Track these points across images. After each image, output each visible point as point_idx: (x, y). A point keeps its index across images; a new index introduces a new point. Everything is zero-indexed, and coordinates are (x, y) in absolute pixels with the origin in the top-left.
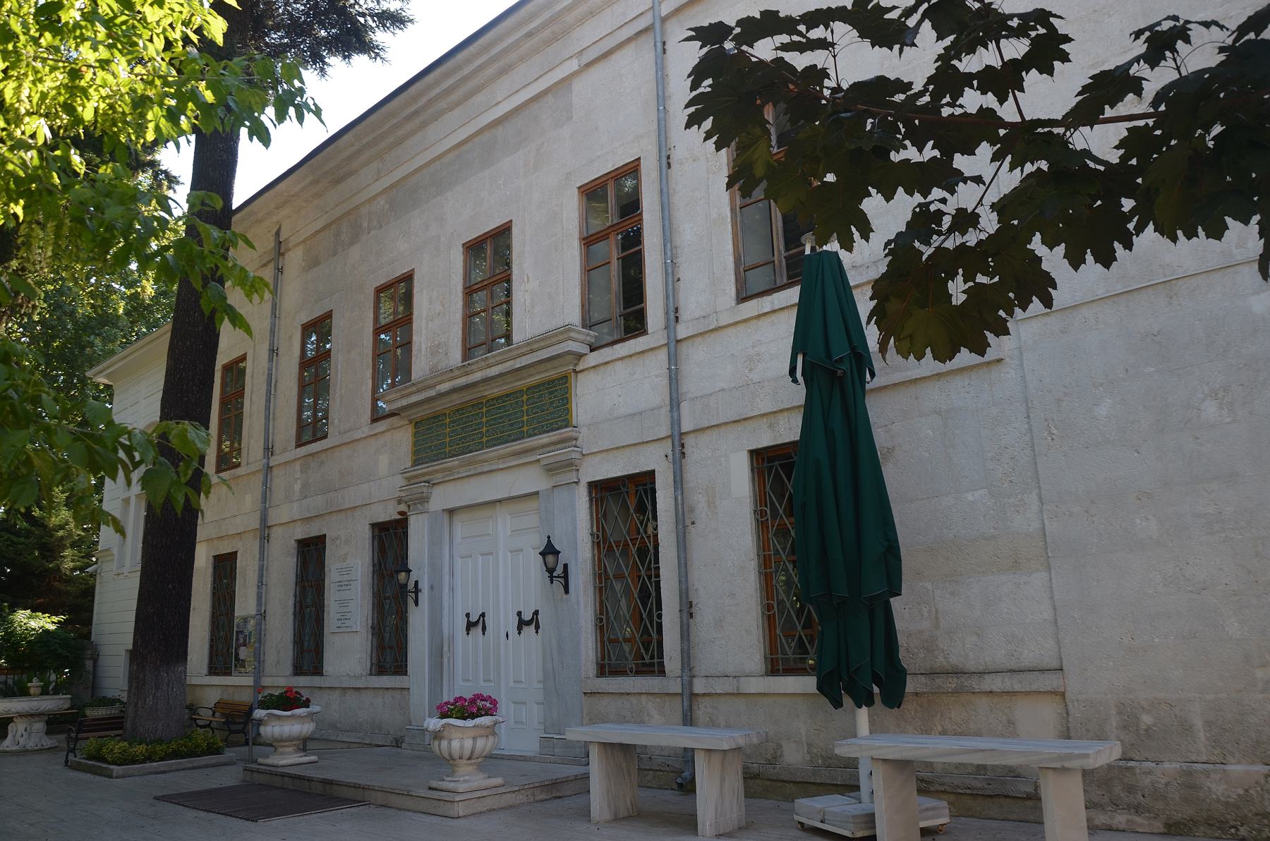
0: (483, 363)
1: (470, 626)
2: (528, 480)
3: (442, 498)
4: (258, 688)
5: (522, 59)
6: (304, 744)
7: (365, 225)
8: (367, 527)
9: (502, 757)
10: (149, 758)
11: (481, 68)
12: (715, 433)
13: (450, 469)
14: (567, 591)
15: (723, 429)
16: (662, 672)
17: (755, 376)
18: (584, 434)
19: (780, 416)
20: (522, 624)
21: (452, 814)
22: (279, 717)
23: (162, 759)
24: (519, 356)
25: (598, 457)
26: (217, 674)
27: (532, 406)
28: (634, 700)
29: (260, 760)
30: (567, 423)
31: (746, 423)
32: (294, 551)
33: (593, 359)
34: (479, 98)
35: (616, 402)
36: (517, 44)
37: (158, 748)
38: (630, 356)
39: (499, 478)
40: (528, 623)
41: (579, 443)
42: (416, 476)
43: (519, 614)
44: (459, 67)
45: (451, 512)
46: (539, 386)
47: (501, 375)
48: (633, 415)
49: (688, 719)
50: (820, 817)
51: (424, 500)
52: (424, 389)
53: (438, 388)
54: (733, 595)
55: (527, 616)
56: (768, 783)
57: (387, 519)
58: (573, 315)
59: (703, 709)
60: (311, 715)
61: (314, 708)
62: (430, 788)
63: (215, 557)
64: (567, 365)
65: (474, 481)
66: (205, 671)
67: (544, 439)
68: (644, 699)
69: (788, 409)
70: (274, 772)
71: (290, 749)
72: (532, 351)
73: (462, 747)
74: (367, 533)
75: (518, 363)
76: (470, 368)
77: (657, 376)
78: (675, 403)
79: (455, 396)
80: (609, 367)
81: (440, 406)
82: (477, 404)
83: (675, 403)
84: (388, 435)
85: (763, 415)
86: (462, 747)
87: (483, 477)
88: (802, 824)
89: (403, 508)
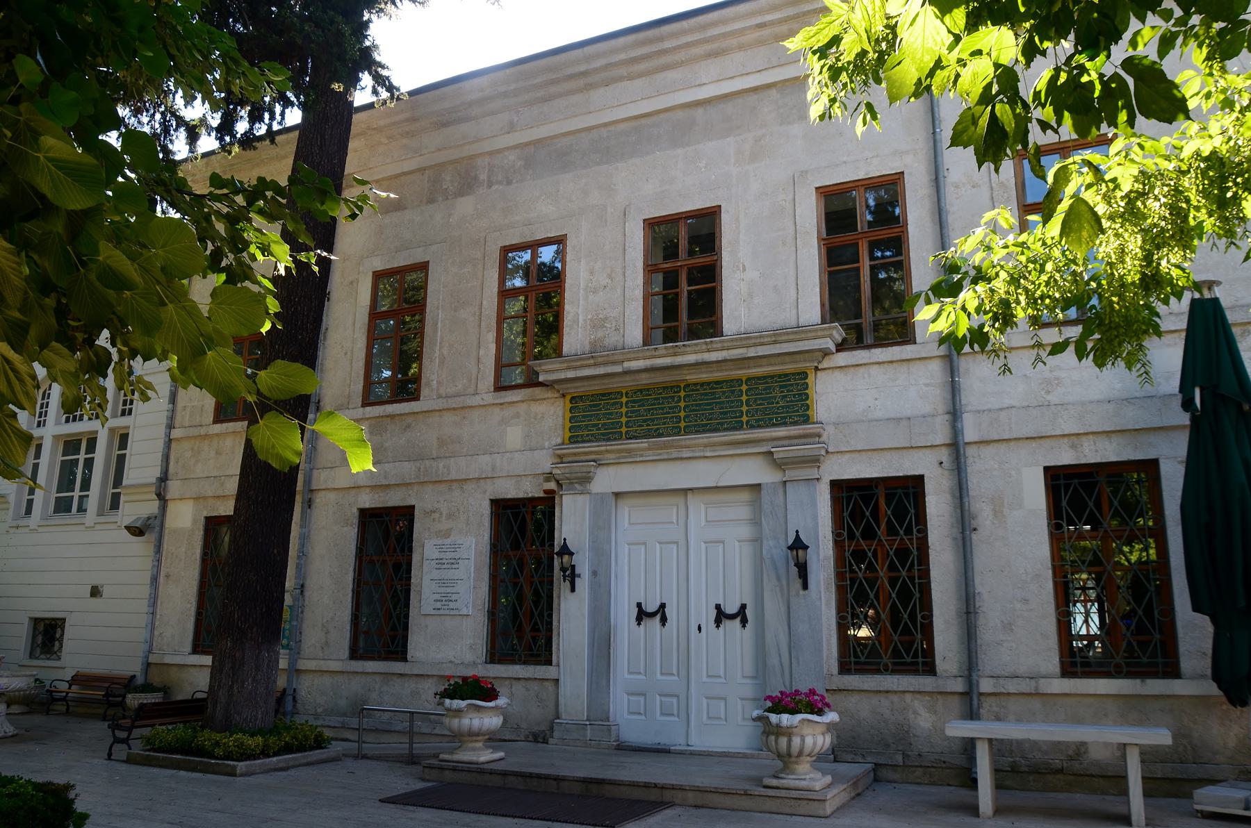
0: (704, 347)
1: (642, 615)
2: (751, 471)
3: (606, 480)
4: (1037, 688)
5: (741, 47)
6: (493, 739)
7: (483, 177)
8: (487, 504)
9: (692, 753)
10: (265, 753)
11: (688, 45)
12: (1003, 446)
13: (629, 451)
14: (805, 586)
15: (1012, 443)
16: (930, 669)
17: (1053, 398)
18: (829, 433)
19: (1084, 438)
20: (721, 616)
21: (821, 813)
22: (479, 708)
23: (275, 754)
24: (755, 345)
25: (847, 456)
26: (500, 662)
27: (773, 397)
28: (895, 698)
29: (442, 756)
30: (806, 420)
31: (1042, 441)
32: (356, 521)
33: (843, 358)
34: (672, 75)
35: (871, 409)
36: (742, 32)
37: (272, 739)
38: (892, 362)
39: (702, 466)
40: (732, 617)
41: (824, 438)
42: (575, 454)
43: (639, 605)
44: (661, 39)
45: (617, 495)
46: (765, 377)
47: (725, 361)
48: (898, 420)
49: (972, 714)
50: (1243, 805)
51: (586, 479)
52: (605, 364)
53: (626, 364)
54: (1026, 601)
55: (731, 609)
56: (1072, 777)
57: (521, 495)
58: (811, 310)
59: (988, 706)
60: (496, 708)
61: (502, 701)
62: (765, 787)
63: (208, 519)
64: (813, 361)
65: (662, 466)
66: (189, 648)
67: (781, 432)
68: (908, 697)
69: (1093, 433)
70: (457, 768)
71: (480, 744)
72: (775, 342)
73: (815, 744)
74: (486, 509)
75: (752, 353)
76: (688, 349)
77: (927, 385)
78: (955, 414)
79: (644, 376)
80: (862, 369)
81: (614, 385)
82: (674, 387)
83: (955, 414)
84: (523, 407)
85: (1064, 436)
86: (815, 744)
87: (678, 463)
88: (1202, 812)
89: (552, 485)
